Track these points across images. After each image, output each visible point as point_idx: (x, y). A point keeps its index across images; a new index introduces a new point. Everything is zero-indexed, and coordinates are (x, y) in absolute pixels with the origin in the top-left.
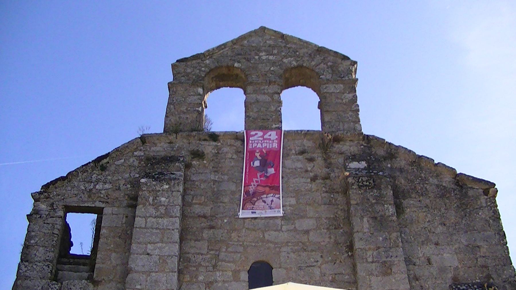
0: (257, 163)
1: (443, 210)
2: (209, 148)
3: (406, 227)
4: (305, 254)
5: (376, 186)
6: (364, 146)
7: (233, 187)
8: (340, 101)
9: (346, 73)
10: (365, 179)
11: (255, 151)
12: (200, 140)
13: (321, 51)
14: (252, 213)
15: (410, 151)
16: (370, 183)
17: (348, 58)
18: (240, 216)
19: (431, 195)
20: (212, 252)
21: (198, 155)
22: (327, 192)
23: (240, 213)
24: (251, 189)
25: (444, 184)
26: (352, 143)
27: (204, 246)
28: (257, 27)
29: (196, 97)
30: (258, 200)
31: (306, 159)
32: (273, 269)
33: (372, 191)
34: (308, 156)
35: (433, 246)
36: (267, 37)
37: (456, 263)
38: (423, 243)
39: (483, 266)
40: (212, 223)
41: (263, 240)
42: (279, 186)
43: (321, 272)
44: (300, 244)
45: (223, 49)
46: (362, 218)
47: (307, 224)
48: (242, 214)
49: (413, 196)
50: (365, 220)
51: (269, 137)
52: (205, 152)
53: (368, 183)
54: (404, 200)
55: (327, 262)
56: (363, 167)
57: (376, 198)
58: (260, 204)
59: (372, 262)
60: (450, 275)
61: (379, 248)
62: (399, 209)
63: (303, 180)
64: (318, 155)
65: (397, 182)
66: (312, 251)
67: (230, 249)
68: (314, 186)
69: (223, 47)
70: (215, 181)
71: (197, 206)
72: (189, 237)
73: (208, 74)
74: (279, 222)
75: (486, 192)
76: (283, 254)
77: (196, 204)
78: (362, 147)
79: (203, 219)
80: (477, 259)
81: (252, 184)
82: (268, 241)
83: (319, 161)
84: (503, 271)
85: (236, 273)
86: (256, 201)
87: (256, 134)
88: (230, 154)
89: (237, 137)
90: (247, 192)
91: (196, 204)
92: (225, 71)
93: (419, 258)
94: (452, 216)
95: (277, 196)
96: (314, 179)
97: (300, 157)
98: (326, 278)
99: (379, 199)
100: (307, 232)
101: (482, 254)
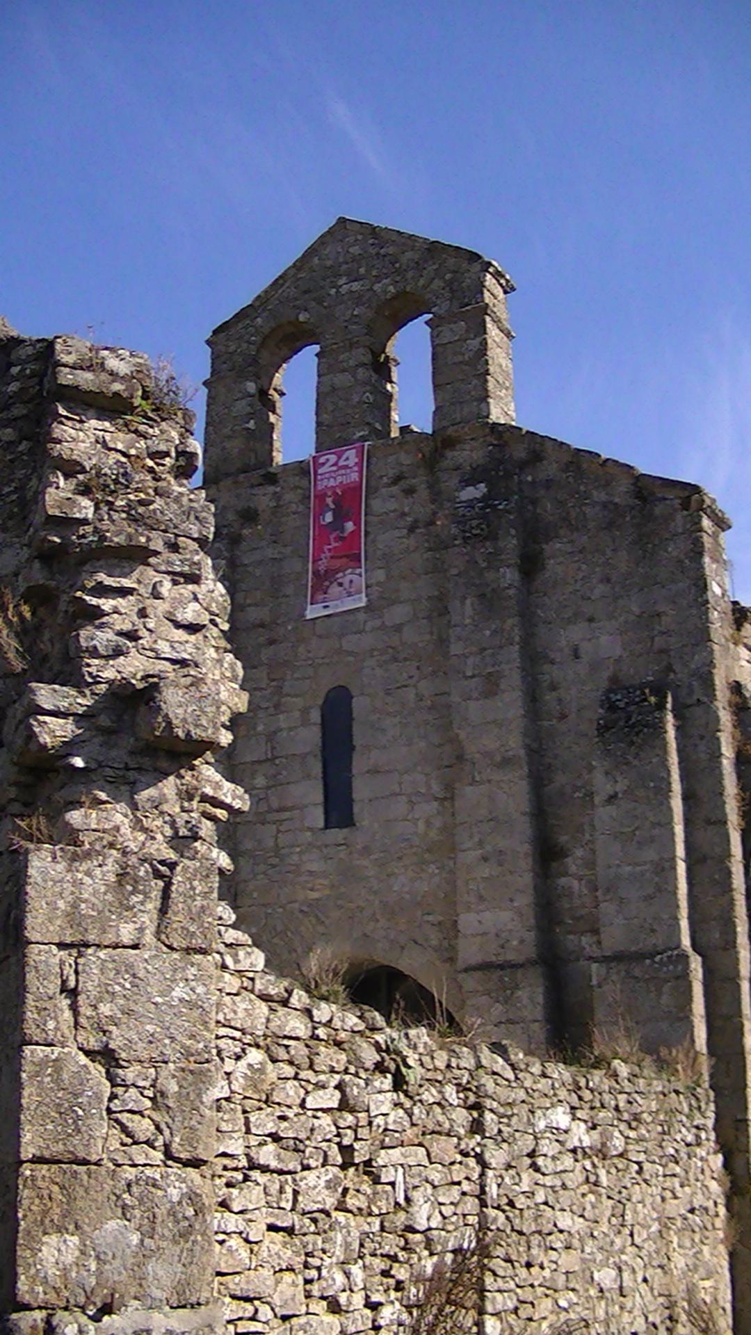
0: (329, 517)
3: (545, 595)
6: (494, 445)
7: (298, 566)
8: (460, 358)
10: (475, 523)
11: (325, 495)
12: (252, 486)
13: (435, 249)
14: (326, 607)
15: (562, 443)
16: (482, 529)
17: (479, 257)
18: (309, 617)
19: (591, 525)
20: (274, 683)
22: (430, 549)
23: (308, 612)
24: (322, 566)
25: (617, 500)
29: (244, 402)
30: (331, 583)
31: (403, 491)
32: (352, 697)
33: (483, 546)
37: (618, 652)
38: (569, 621)
39: (661, 651)
42: (360, 553)
43: (417, 694)
44: (390, 650)
45: (282, 285)
47: (398, 614)
48: (312, 612)
49: (562, 532)
50: (468, 602)
51: (345, 463)
52: (260, 509)
53: (478, 532)
54: (547, 543)
56: (478, 495)
58: (335, 590)
59: (473, 676)
60: (606, 674)
62: (530, 565)
63: (397, 533)
64: (420, 481)
65: (538, 511)
66: (406, 659)
67: (295, 676)
68: (411, 542)
69: (281, 282)
73: (263, 344)
74: (361, 616)
75: (686, 504)
76: (366, 671)
77: (249, 605)
78: (491, 448)
79: (261, 629)
80: (652, 639)
81: (323, 556)
82: (350, 653)
83: (423, 493)
84: (694, 655)
85: (305, 711)
86: (328, 587)
87: (328, 460)
88: (294, 505)
89: (301, 469)
91: (249, 605)
93: (561, 650)
94: (623, 560)
95: (358, 571)
96: (412, 529)
98: (423, 704)
99: (494, 560)
100: (398, 628)
101: (663, 629)
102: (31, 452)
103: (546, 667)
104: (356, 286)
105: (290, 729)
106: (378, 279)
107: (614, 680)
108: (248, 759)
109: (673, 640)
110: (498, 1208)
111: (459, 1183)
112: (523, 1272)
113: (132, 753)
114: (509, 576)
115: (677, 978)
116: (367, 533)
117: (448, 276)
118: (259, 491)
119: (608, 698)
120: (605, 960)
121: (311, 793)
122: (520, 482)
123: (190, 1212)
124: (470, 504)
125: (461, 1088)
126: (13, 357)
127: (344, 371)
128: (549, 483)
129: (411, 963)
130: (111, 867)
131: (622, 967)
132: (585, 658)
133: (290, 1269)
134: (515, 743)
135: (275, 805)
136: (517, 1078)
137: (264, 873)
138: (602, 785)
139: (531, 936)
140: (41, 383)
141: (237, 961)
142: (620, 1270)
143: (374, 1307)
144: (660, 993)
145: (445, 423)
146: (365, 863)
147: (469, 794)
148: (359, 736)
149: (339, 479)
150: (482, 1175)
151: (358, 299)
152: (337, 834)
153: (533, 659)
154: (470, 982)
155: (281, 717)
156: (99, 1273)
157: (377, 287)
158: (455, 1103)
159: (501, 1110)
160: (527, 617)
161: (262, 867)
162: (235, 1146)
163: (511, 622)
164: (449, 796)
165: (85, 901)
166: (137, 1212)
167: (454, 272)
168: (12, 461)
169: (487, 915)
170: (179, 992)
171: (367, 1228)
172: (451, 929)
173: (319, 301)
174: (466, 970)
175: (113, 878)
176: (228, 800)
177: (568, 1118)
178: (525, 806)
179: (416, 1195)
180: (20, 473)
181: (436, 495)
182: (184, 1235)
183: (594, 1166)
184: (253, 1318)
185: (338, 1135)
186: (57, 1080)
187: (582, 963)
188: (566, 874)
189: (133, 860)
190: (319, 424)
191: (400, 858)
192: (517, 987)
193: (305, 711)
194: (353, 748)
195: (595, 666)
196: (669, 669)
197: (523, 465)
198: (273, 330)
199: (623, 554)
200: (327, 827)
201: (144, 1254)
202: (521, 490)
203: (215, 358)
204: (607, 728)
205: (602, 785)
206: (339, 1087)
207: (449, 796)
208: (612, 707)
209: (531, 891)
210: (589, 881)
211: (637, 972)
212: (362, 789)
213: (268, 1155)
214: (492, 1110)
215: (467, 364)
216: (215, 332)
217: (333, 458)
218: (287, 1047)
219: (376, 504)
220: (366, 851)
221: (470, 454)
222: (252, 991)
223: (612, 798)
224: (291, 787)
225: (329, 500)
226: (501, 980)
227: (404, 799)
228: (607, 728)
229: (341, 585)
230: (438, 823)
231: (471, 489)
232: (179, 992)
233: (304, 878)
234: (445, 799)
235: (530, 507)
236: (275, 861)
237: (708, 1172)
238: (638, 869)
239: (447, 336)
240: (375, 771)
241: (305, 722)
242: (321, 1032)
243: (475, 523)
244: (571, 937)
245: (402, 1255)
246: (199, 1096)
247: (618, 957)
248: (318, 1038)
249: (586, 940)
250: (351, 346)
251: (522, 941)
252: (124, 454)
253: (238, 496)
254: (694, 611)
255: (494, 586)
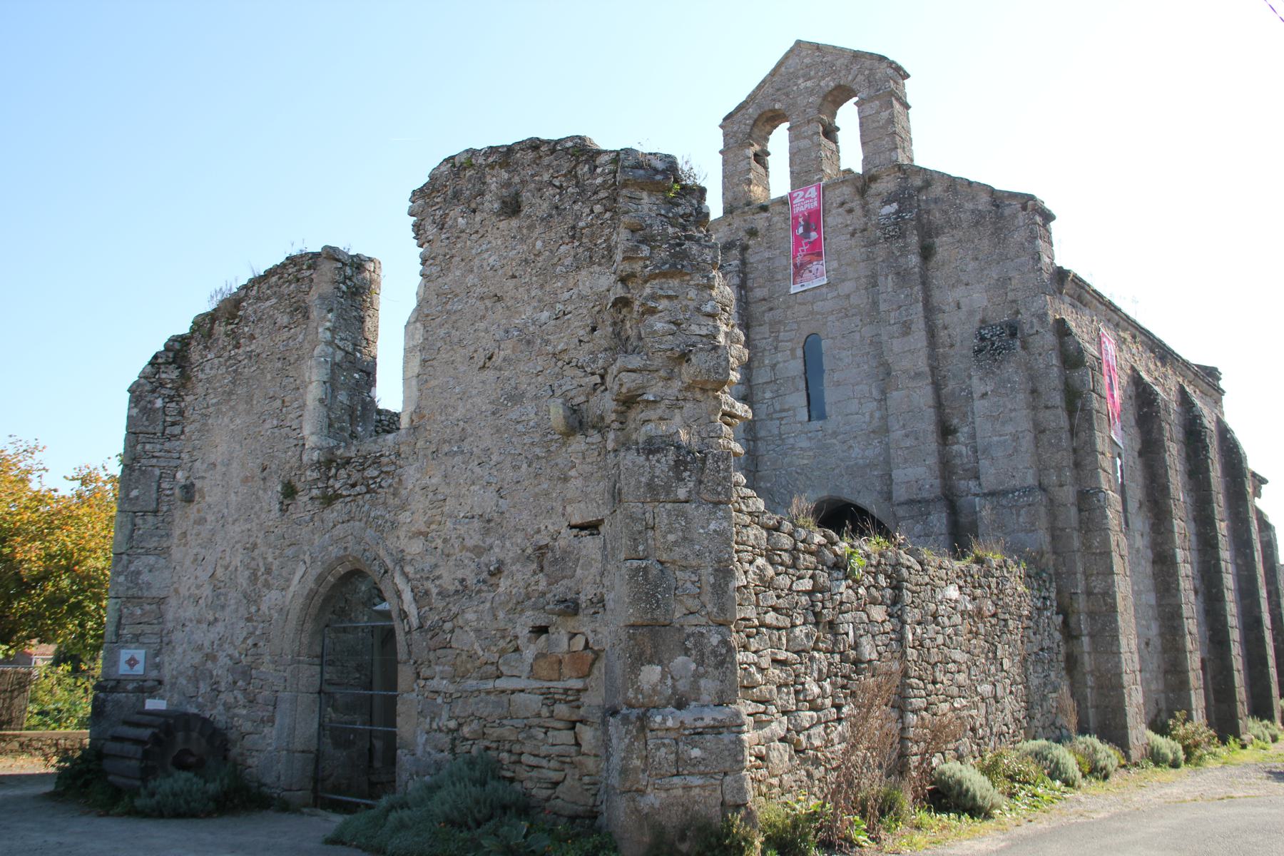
0: (801, 230)
1: (976, 241)
2: (760, 221)
4: (846, 320)
5: (902, 235)
7: (784, 262)
9: (57, 702)
10: (890, 228)
13: (857, 56)
17: (886, 58)
19: (965, 225)
21: (752, 233)
24: (798, 261)
25: (980, 208)
26: (889, 178)
27: (766, 329)
28: (792, 44)
34: (847, 206)
35: (964, 287)
36: (804, 54)
40: (771, 305)
41: (812, 313)
46: (887, 276)
47: (847, 287)
50: (890, 278)
55: (865, 325)
56: (893, 211)
57: (900, 249)
58: (806, 275)
61: (900, 307)
62: (927, 252)
63: (843, 238)
64: (856, 204)
66: (853, 315)
68: (853, 242)
70: (769, 259)
71: (593, 400)
72: (754, 324)
74: (824, 290)
82: (818, 313)
83: (858, 211)
85: (793, 350)
89: (783, 201)
90: (795, 265)
92: (771, 114)
93: (949, 304)
97: (840, 210)
99: (904, 251)
100: (848, 296)
102: (612, 218)
103: (940, 315)
104: (809, 84)
105: (785, 362)
106: (823, 78)
107: (983, 321)
108: (760, 381)
109: (1020, 294)
110: (914, 647)
111: (888, 633)
112: (930, 687)
113: (680, 391)
114: (914, 260)
115: (1029, 505)
116: (825, 239)
117: (867, 72)
118: (756, 217)
119: (980, 333)
120: (985, 495)
121: (799, 399)
122: (918, 200)
123: (724, 651)
124: (888, 216)
125: (888, 576)
126: (597, 163)
127: (805, 138)
128: (936, 201)
129: (867, 501)
130: (671, 456)
131: (994, 499)
132: (964, 309)
133: (786, 685)
134: (922, 365)
135: (778, 407)
136: (923, 570)
137: (773, 450)
138: (978, 386)
139: (937, 482)
140: (615, 177)
141: (747, 507)
142: (995, 685)
143: (839, 707)
144: (1018, 515)
145: (870, 166)
146: (834, 441)
147: (895, 396)
148: (826, 363)
149: (806, 206)
150: (902, 627)
151: (811, 92)
152: (816, 424)
153: (930, 310)
154: (901, 512)
155: (779, 355)
156: (674, 687)
157: (822, 84)
158: (884, 585)
159: (914, 588)
160: (925, 283)
161: (772, 447)
162: (750, 612)
163: (917, 288)
164: (883, 399)
165: (657, 477)
166: (693, 652)
167: (871, 69)
168: (602, 224)
169: (910, 470)
170: (712, 527)
171: (831, 660)
172: (888, 478)
173: (787, 95)
174: (898, 505)
175: (672, 463)
176: (739, 413)
177: (958, 592)
178: (931, 402)
179: (864, 640)
180: (607, 231)
181: (867, 212)
182: (722, 663)
183: (975, 622)
184: (764, 713)
185: (812, 606)
186: (646, 579)
187: (969, 497)
188: (958, 443)
189: (683, 452)
190: (792, 172)
191: (855, 437)
192: (929, 514)
193: (793, 350)
194: (824, 371)
195: (971, 313)
196: (1018, 312)
197: (919, 190)
198: (760, 116)
199: (986, 242)
200: (810, 420)
201: (697, 676)
202: (919, 206)
203: (725, 135)
204: (980, 351)
205: (978, 386)
206: (812, 577)
207: (883, 399)
208: (983, 339)
209: (936, 454)
210: (972, 447)
211: (1004, 502)
212: (830, 396)
213: (771, 618)
214: (907, 589)
215: (881, 128)
216: (725, 119)
217: (801, 193)
218: (780, 555)
219: (829, 220)
220: (835, 434)
221: (886, 185)
222: (758, 524)
223: (984, 395)
224: (787, 397)
225: (801, 220)
226: (920, 510)
227: (856, 401)
228: (980, 351)
229: (810, 271)
230: (877, 415)
231: (887, 207)
232: (712, 527)
233: (797, 452)
234: (881, 400)
235: (925, 216)
236: (779, 442)
237: (1052, 626)
238: (1002, 438)
239: (868, 112)
240: (838, 384)
241: (794, 357)
242: (801, 545)
243: (890, 228)
244: (963, 482)
245: (854, 676)
246: (727, 585)
247: (992, 494)
248: (799, 551)
249: (972, 484)
250: (809, 122)
251: (931, 486)
252: (666, 217)
253: (745, 221)
254: (1032, 275)
255: (905, 266)
